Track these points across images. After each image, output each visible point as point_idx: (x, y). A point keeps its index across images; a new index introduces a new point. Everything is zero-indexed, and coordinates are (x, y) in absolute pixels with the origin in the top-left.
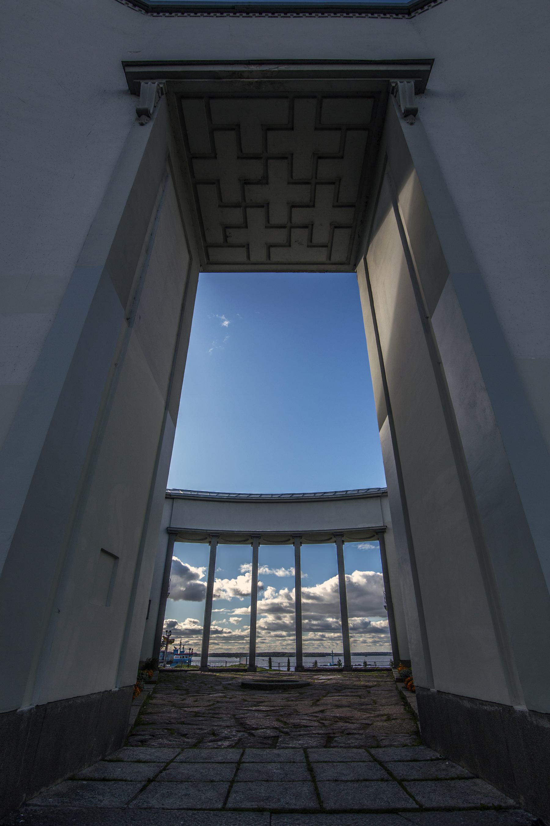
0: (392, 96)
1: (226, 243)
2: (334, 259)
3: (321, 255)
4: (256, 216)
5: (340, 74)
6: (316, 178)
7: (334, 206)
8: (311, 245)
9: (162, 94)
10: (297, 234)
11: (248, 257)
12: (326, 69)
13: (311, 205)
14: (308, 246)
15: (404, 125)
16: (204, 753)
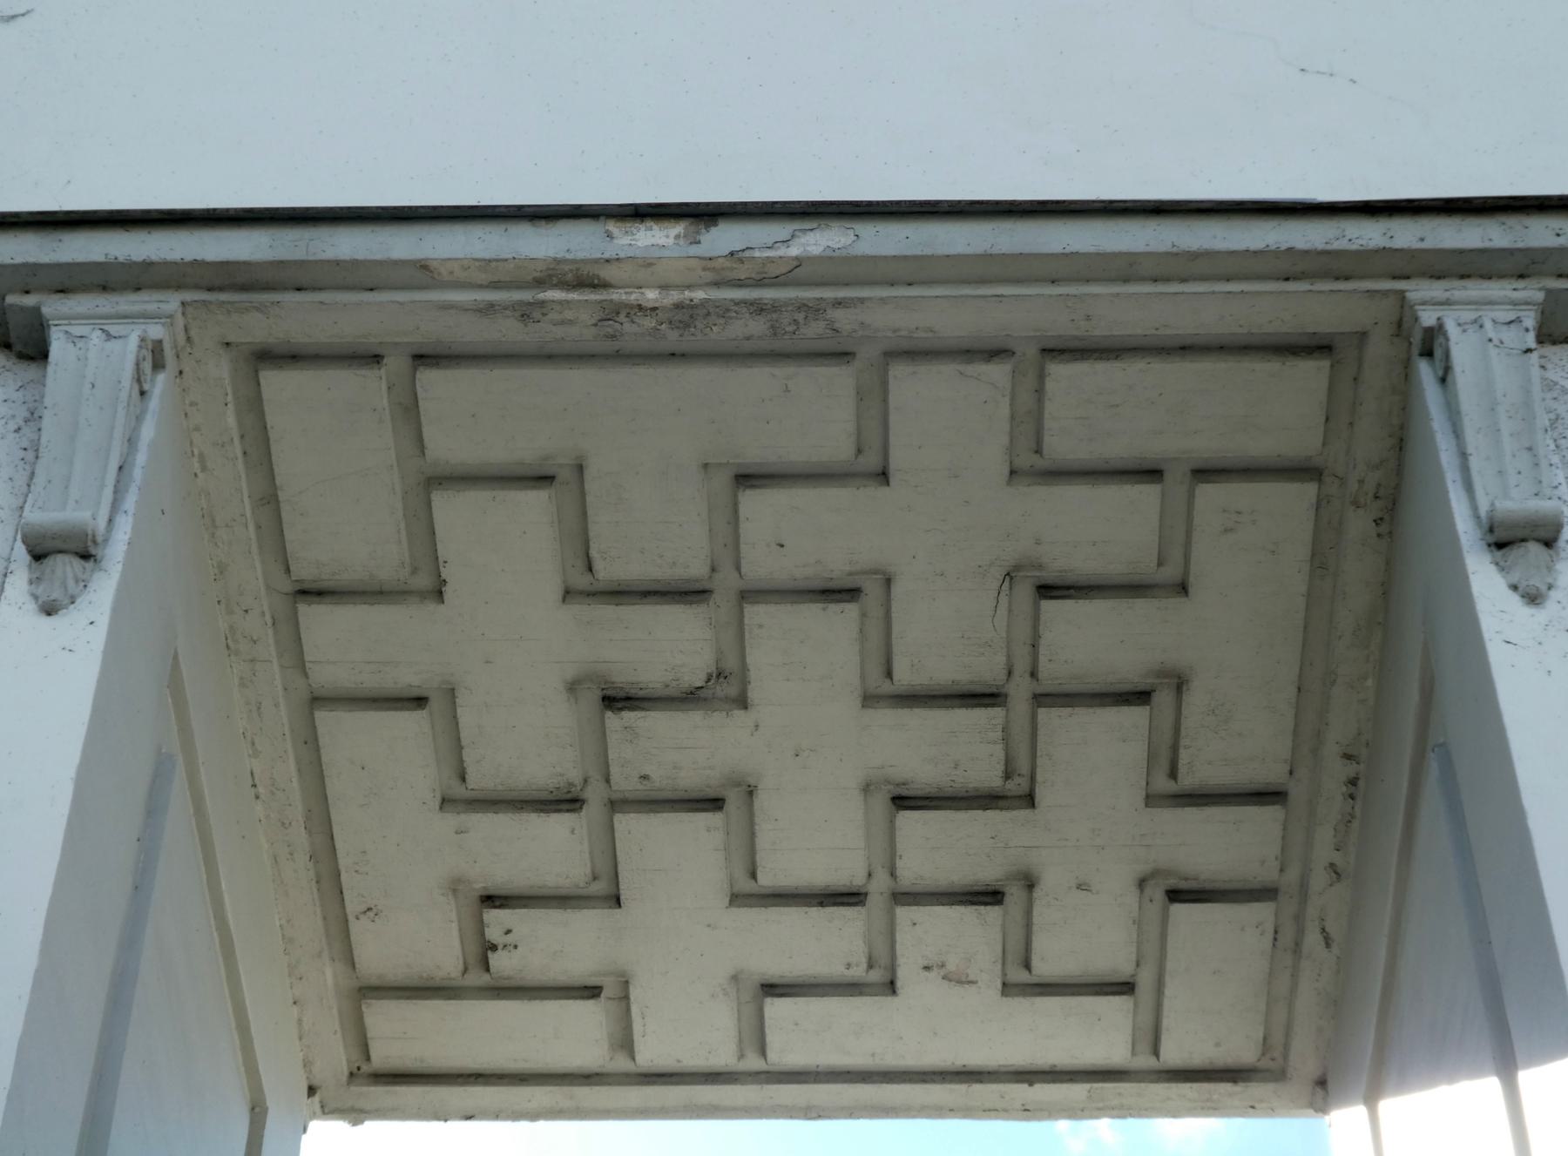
0: (1425, 372)
1: (483, 978)
2: (1174, 1053)
3: (1101, 1033)
4: (675, 860)
5: (1125, 269)
6: (1033, 674)
7: (1151, 800)
8: (1026, 983)
9: (158, 365)
10: (929, 933)
11: (625, 1042)
12: (1056, 248)
13: (1014, 794)
14: (1008, 989)
15: (1486, 582)
16: (675, 296)
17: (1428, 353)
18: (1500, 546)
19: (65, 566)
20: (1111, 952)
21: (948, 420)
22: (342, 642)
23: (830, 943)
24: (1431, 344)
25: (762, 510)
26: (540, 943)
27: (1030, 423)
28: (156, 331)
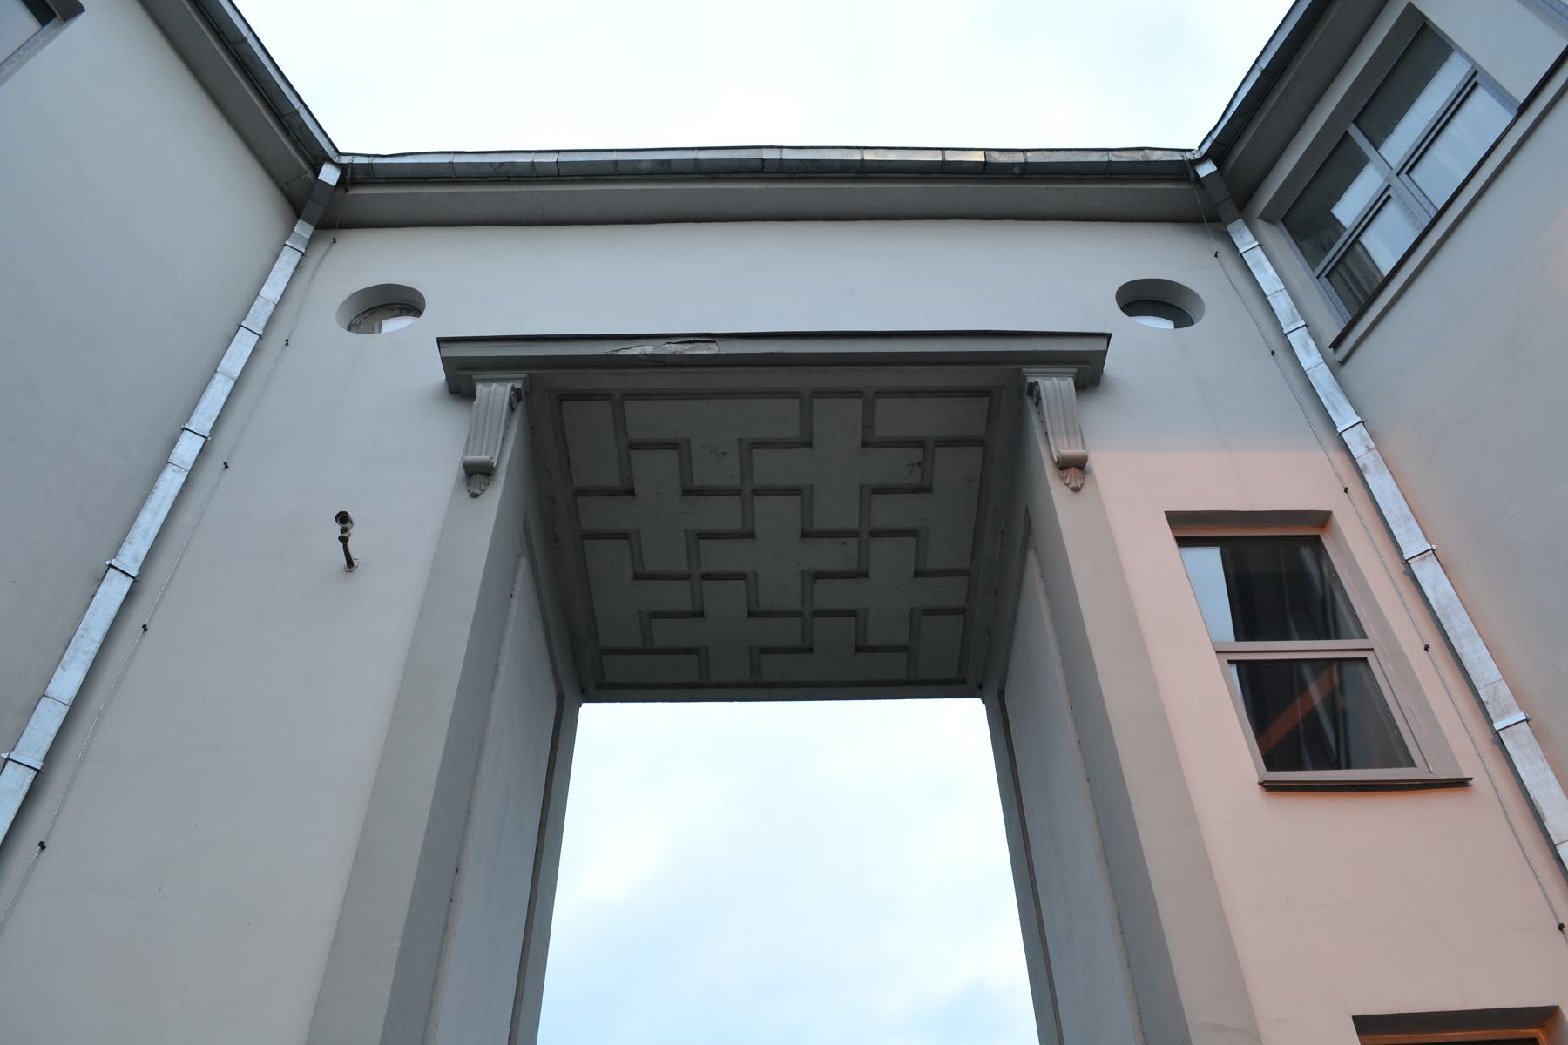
0: (1030, 403)
10: (727, 473)
17: (1030, 394)
18: (1062, 469)
19: (478, 478)
20: (642, 461)
21: (838, 422)
22: (598, 514)
23: (770, 467)
24: (1032, 390)
25: (761, 458)
26: (896, 466)
27: (867, 424)
28: (518, 385)
